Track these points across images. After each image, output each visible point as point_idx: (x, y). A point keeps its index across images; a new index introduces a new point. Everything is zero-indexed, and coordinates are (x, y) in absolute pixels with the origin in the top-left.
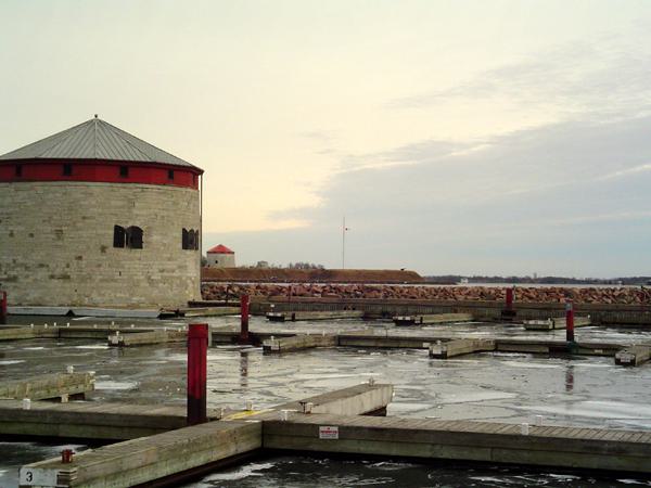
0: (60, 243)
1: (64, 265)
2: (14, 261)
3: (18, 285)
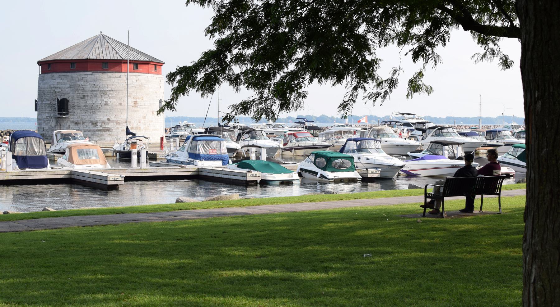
0: (136, 109)
1: (138, 122)
2: (108, 120)
3: (111, 133)
